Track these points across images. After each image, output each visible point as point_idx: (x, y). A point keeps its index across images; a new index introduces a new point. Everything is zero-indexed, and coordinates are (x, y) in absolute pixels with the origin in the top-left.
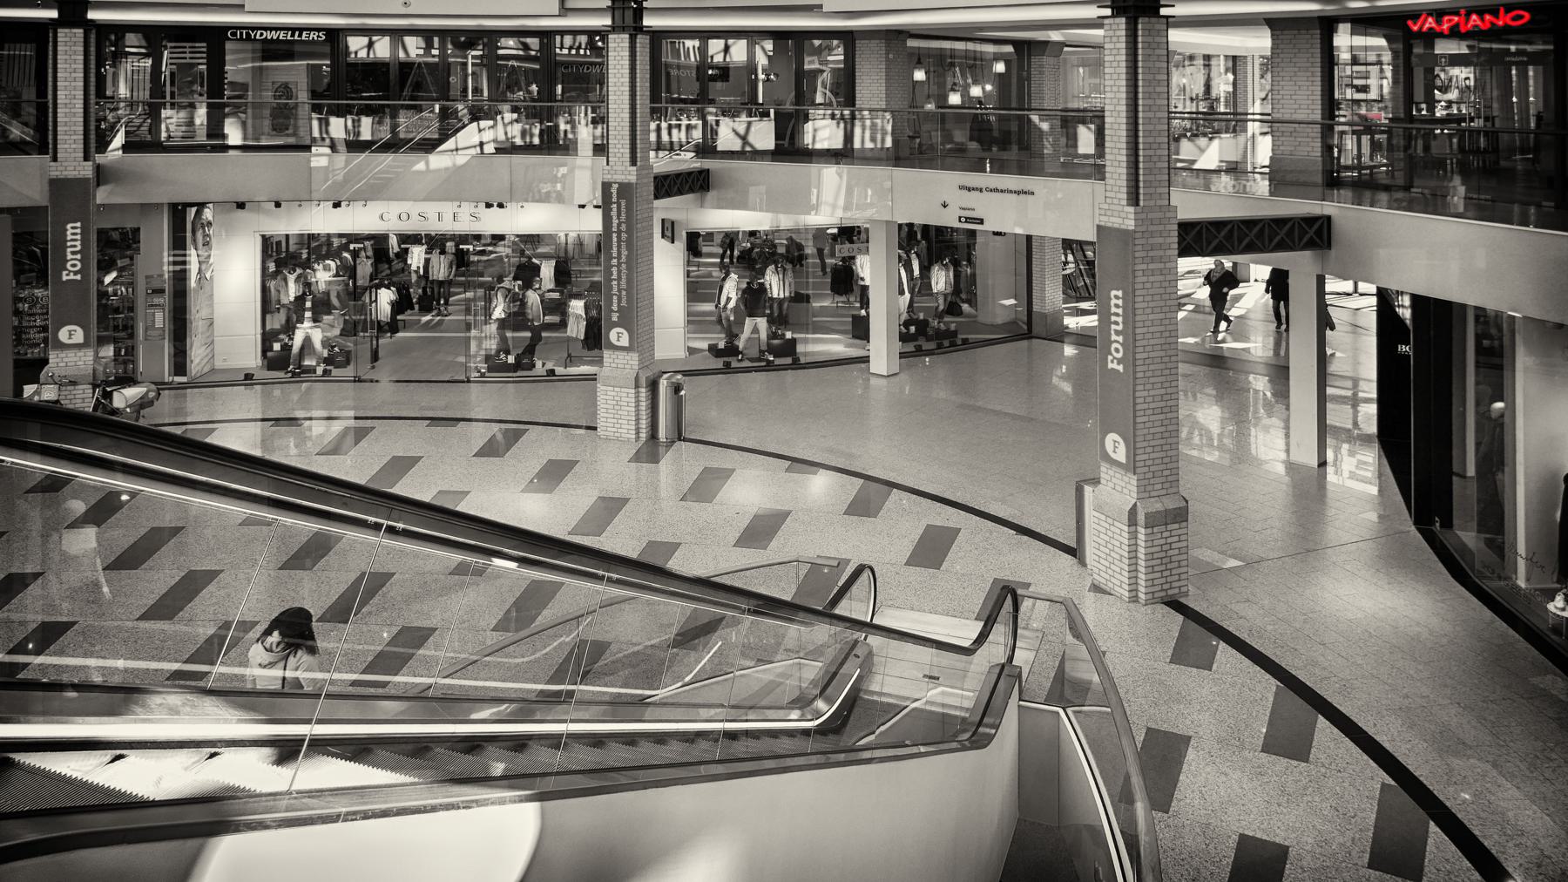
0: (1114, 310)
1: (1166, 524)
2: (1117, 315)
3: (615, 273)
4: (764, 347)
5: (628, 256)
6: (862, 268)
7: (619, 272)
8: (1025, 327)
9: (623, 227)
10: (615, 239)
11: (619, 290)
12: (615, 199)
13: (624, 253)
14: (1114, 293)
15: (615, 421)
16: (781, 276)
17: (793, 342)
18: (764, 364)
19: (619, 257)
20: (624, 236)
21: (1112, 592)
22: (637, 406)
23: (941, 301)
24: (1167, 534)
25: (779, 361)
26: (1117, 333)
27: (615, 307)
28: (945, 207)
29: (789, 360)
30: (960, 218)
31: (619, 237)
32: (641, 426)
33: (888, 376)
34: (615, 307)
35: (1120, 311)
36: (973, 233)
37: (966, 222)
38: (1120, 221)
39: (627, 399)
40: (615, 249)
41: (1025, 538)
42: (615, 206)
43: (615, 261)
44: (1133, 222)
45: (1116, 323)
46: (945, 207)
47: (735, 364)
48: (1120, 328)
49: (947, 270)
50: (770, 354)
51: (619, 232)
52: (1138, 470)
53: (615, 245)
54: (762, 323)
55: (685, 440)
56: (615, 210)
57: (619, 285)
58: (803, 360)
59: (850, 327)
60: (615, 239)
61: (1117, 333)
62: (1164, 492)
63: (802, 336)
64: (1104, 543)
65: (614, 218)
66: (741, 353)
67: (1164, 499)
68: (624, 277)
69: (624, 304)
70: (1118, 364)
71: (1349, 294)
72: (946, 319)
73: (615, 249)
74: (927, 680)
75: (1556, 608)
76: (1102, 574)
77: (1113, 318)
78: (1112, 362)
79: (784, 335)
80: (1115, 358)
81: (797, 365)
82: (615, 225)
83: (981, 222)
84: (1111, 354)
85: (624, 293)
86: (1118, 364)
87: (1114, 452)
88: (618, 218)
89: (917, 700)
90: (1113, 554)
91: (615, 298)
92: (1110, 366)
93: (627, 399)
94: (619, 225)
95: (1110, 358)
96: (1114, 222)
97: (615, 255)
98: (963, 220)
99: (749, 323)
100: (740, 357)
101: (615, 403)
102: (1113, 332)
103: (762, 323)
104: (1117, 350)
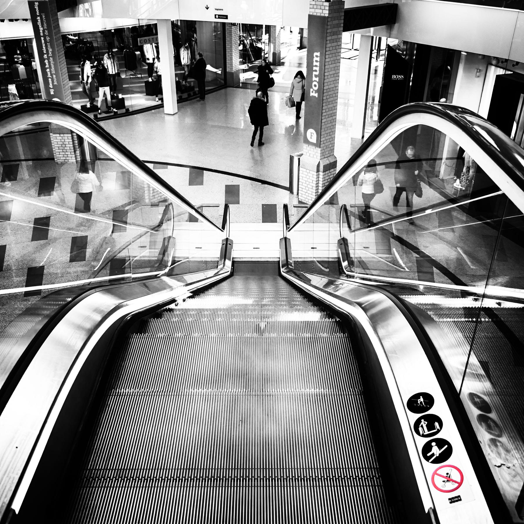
0: (315, 63)
1: (330, 170)
2: (316, 66)
3: (47, 64)
4: (110, 104)
5: (52, 52)
6: (147, 52)
7: (49, 63)
8: (223, 82)
9: (46, 33)
10: (43, 41)
11: (51, 75)
12: (38, 14)
13: (50, 50)
14: (315, 54)
15: (64, 153)
16: (112, 60)
17: (123, 99)
18: (112, 114)
19: (47, 53)
20: (48, 38)
21: (307, 203)
22: (73, 143)
23: (186, 69)
24: (329, 174)
25: (120, 112)
26: (316, 76)
27: (51, 86)
28: (207, 8)
29: (124, 111)
30: (215, 15)
31: (45, 40)
32: (77, 154)
33: (174, 114)
34: (51, 86)
35: (318, 64)
36: (224, 24)
37: (219, 18)
38: (321, 11)
39: (68, 140)
40: (44, 48)
41: (266, 185)
42: (39, 18)
43: (45, 56)
44: (327, 12)
45: (316, 71)
46: (207, 8)
47: (99, 116)
48: (317, 73)
49: (188, 50)
50: (114, 108)
51: (44, 36)
52: (321, 146)
53: (44, 45)
54: (107, 89)
55: (100, 159)
56: (39, 21)
57: (50, 71)
58: (131, 110)
59: (145, 90)
60: (43, 41)
61: (316, 76)
62: (329, 155)
63: (129, 96)
64: (305, 182)
65: (40, 26)
66: (99, 109)
67: (330, 158)
68: (53, 66)
69: (55, 83)
70: (315, 93)
71: (351, 49)
72: (188, 80)
73: (44, 48)
74: (140, 248)
75: (457, 185)
76: (303, 196)
77: (314, 68)
78: (312, 92)
79: (118, 96)
80: (314, 90)
81: (129, 113)
82: (41, 31)
83: (226, 17)
84: (312, 88)
85: (54, 76)
86: (315, 93)
87: (311, 138)
88: (43, 26)
89: (136, 257)
90: (308, 186)
91: (50, 80)
92: (311, 94)
93: (68, 140)
94: (44, 31)
95: (311, 90)
96: (318, 12)
97: (45, 52)
98: (217, 16)
99: (101, 90)
100: (100, 111)
101: (62, 143)
102: (314, 76)
103: (107, 89)
104: (315, 86)
